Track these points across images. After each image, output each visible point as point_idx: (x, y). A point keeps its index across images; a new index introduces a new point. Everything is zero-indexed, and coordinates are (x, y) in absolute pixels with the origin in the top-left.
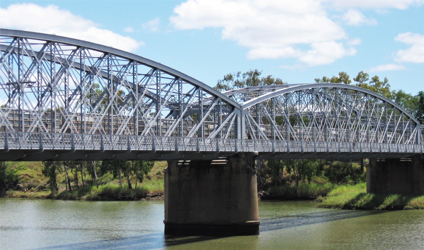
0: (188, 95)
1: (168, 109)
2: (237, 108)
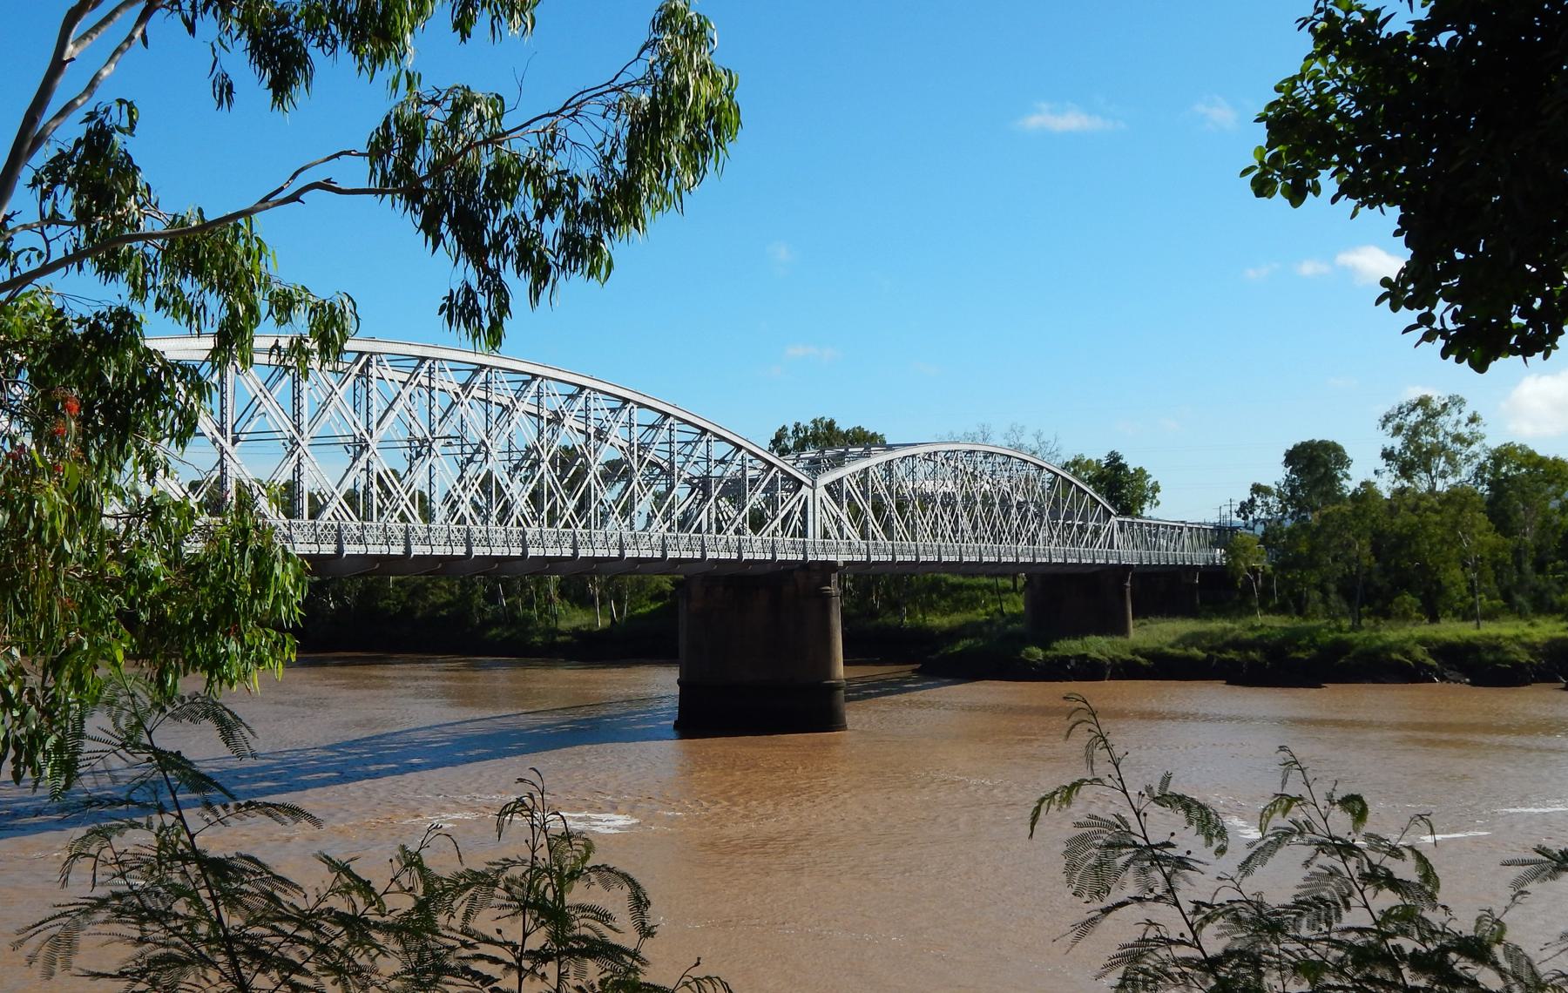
0: (722, 461)
1: (687, 485)
2: (808, 486)
